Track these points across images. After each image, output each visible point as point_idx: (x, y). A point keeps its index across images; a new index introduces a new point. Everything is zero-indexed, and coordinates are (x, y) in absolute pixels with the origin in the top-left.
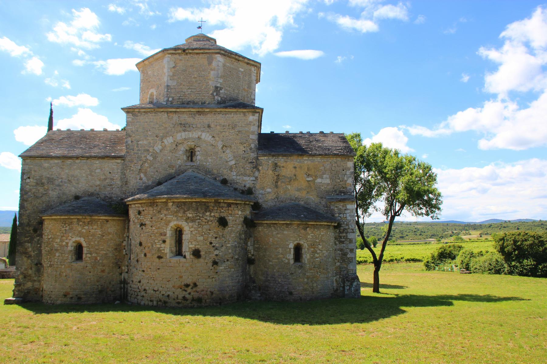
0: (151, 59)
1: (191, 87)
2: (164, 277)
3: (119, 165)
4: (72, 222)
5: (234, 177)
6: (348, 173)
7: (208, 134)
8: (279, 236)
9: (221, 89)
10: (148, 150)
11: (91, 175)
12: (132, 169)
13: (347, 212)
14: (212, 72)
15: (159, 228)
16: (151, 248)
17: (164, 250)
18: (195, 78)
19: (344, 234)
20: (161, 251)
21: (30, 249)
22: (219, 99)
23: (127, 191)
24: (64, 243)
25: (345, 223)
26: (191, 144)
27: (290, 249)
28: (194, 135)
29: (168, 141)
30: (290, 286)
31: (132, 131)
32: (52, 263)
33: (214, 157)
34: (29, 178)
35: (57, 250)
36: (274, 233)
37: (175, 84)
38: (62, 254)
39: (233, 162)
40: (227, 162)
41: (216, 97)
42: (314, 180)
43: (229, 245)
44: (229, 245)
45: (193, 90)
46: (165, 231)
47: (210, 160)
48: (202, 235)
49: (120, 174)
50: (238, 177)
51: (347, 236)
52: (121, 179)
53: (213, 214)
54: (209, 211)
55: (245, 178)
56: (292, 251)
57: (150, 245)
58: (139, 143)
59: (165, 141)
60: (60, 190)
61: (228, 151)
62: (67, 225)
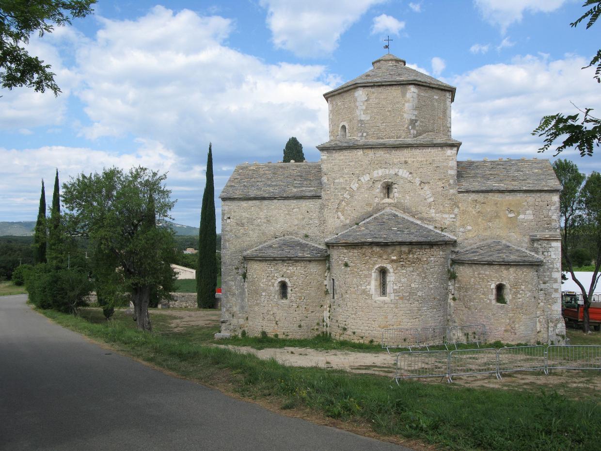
2: (370, 317)
5: (433, 215)
6: (552, 208)
7: (405, 171)
9: (416, 121)
13: (550, 249)
14: (407, 105)
17: (369, 291)
18: (389, 111)
19: (548, 273)
20: (367, 292)
21: (234, 287)
22: (415, 132)
25: (550, 261)
28: (391, 172)
30: (491, 326)
32: (258, 302)
33: (412, 194)
34: (229, 218)
35: (264, 291)
37: (368, 118)
39: (432, 199)
40: (425, 199)
41: (412, 131)
42: (516, 217)
43: (431, 286)
44: (431, 286)
48: (406, 277)
51: (551, 275)
53: (415, 257)
54: (413, 253)
55: (444, 216)
56: (494, 291)
60: (260, 230)
61: (426, 187)
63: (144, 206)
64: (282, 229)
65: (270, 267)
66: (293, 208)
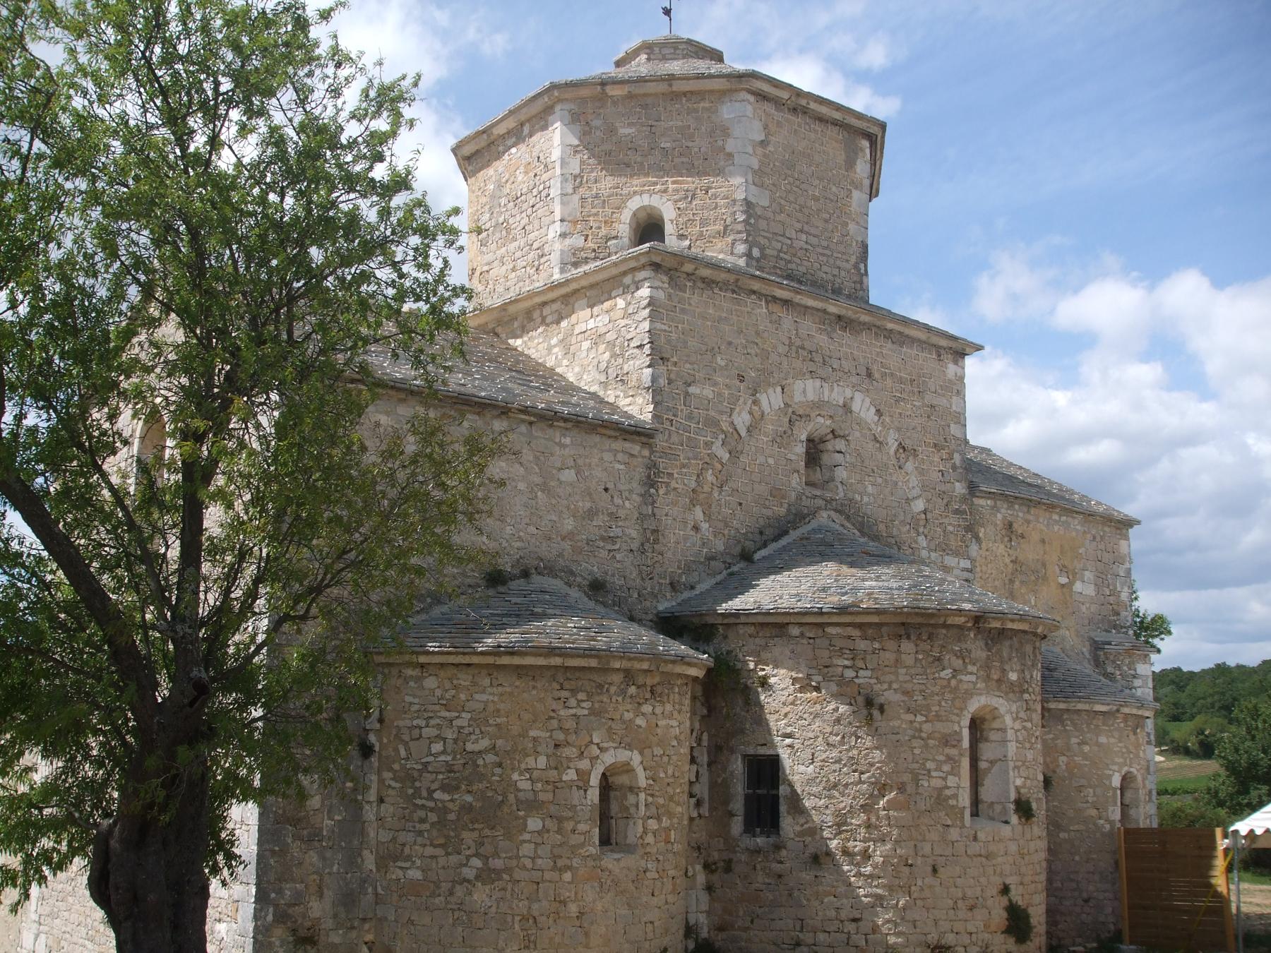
0: (585, 92)
1: (806, 228)
3: (635, 462)
4: (600, 686)
8: (1086, 748)
10: (716, 424)
11: (545, 488)
12: (673, 484)
15: (938, 717)
16: (910, 789)
17: (955, 796)
23: (658, 569)
24: (570, 775)
26: (821, 424)
27: (1115, 789)
28: (834, 395)
29: (771, 400)
31: (669, 342)
35: (533, 805)
36: (1074, 740)
38: (560, 820)
39: (919, 505)
42: (1071, 584)
45: (814, 241)
46: (957, 728)
47: (870, 489)
49: (639, 499)
50: (933, 555)
52: (642, 517)
57: (906, 778)
58: (692, 390)
59: (763, 398)
62: (581, 696)
63: (645, 292)
64: (518, 544)
65: (573, 702)
66: (558, 465)
